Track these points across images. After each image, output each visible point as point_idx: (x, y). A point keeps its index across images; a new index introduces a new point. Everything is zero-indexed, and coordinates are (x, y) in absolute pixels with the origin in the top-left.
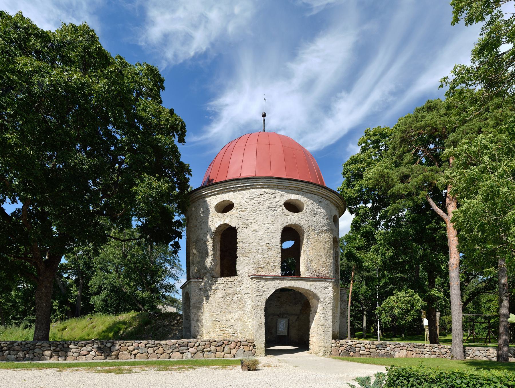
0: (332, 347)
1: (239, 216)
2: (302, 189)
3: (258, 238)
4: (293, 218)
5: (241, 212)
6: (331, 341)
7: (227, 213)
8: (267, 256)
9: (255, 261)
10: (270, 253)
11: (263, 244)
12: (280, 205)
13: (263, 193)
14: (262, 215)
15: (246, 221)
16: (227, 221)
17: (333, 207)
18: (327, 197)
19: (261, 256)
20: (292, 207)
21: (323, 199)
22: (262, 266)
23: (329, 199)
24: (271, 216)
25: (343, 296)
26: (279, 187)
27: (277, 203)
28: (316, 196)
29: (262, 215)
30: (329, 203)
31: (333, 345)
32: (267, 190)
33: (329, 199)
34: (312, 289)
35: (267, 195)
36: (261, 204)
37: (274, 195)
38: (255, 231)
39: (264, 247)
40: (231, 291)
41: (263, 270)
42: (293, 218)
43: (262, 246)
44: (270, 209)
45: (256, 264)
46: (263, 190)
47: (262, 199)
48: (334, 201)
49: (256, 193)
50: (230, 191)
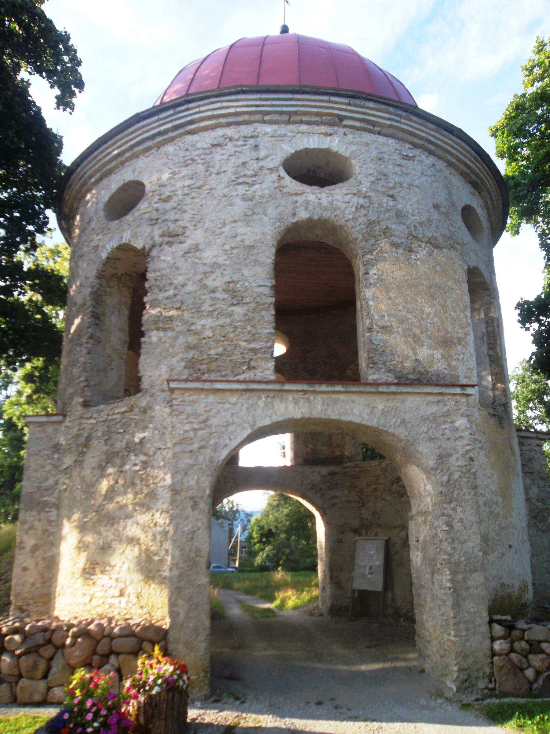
0: (493, 654)
1: (155, 215)
2: (341, 118)
3: (201, 269)
4: (313, 202)
5: (161, 205)
6: (485, 628)
7: (129, 217)
8: (228, 320)
9: (191, 339)
10: (239, 310)
11: (217, 283)
12: (271, 166)
13: (220, 140)
14: (215, 202)
15: (170, 224)
16: (126, 237)
17: (456, 181)
18: (431, 147)
19: (208, 322)
20: (316, 171)
21: (417, 152)
22: (212, 352)
23: (439, 152)
24: (243, 199)
25: (530, 460)
26: (267, 118)
27: (261, 163)
28: (391, 141)
29: (215, 202)
30: (441, 165)
31: (498, 646)
32: (230, 132)
33: (439, 152)
34: (392, 426)
35: (230, 146)
36: (214, 171)
37: (251, 141)
38: (196, 248)
39: (220, 295)
40: (120, 445)
41: (213, 366)
42: (313, 202)
43: (213, 291)
44: (241, 180)
45: (195, 347)
46: (220, 132)
47: (218, 156)
48: (459, 160)
49: (199, 145)
50: (136, 156)
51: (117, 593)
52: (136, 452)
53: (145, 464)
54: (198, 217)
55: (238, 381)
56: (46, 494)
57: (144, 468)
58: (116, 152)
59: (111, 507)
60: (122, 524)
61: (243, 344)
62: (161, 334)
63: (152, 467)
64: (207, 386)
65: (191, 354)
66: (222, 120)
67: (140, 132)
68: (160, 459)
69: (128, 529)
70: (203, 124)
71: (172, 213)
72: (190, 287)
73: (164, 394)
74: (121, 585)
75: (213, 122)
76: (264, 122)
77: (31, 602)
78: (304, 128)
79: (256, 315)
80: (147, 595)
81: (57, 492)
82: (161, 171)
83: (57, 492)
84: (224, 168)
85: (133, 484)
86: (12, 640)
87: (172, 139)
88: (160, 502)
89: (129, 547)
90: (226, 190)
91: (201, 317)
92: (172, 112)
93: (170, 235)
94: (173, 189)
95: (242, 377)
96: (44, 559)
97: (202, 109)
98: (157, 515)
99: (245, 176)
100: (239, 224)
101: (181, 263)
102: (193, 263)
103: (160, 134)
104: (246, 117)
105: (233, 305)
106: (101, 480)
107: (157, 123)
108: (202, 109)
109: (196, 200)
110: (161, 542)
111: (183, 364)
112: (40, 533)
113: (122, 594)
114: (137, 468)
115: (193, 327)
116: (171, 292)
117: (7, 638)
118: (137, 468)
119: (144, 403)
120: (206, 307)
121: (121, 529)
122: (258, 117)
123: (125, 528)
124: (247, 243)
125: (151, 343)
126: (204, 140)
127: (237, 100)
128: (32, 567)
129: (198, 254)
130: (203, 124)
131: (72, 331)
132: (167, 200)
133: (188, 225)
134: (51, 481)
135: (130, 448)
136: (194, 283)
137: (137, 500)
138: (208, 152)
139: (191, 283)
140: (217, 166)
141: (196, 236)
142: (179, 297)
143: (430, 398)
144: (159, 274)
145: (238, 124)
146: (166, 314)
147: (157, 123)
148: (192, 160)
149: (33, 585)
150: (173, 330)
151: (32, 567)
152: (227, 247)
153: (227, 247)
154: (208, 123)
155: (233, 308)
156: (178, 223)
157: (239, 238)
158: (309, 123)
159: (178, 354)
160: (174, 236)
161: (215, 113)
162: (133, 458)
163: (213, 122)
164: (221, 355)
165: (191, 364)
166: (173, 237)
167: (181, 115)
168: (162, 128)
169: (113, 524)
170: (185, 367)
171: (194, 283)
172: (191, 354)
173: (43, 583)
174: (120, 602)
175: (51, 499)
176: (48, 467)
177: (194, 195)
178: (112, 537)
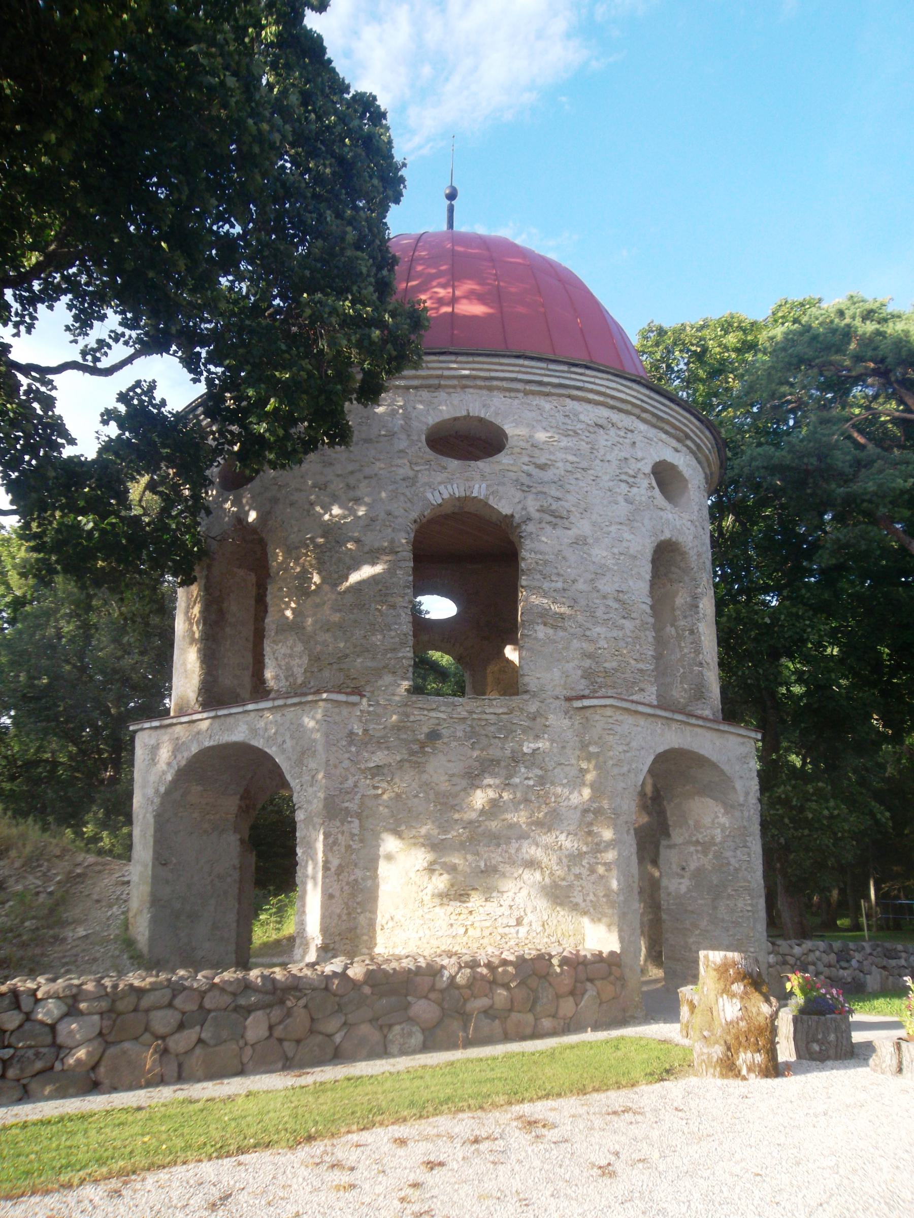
8: (621, 634)
9: (588, 647)
15: (550, 500)
26: (644, 415)
32: (615, 417)
35: (613, 432)
44: (623, 477)
47: (602, 440)
49: (582, 417)
51: (513, 922)
52: (527, 764)
53: (542, 781)
54: (583, 505)
55: (632, 702)
56: (347, 798)
57: (543, 784)
58: (467, 372)
59: (494, 825)
60: (514, 845)
61: (633, 662)
62: (550, 631)
63: (553, 783)
64: (633, 707)
65: (587, 663)
66: (611, 402)
67: (517, 369)
68: (562, 776)
69: (524, 851)
70: (591, 396)
71: (553, 486)
72: (581, 586)
73: (557, 702)
74: (516, 914)
75: (601, 399)
76: (638, 417)
77: (337, 939)
78: (664, 436)
79: (642, 635)
80: (555, 922)
81: (358, 796)
82: (533, 427)
83: (358, 796)
84: (608, 457)
85: (527, 801)
86: (505, 972)
87: (548, 394)
88: (566, 823)
89: (527, 871)
90: (611, 484)
91: (596, 623)
92: (565, 368)
93: (553, 513)
94: (552, 457)
95: (634, 698)
96: (348, 883)
97: (597, 381)
98: (562, 837)
99: (626, 473)
100: (624, 528)
101: (568, 553)
102: (582, 557)
103: (540, 383)
104: (629, 407)
105: (624, 618)
106: (471, 792)
107: (543, 372)
108: (597, 381)
109: (581, 484)
110: (569, 867)
111: (580, 672)
112: (343, 850)
113: (519, 922)
114: (531, 783)
115: (588, 633)
116: (560, 585)
117: (500, 970)
118: (531, 783)
119: (533, 708)
120: (599, 613)
121: (513, 851)
122: (637, 411)
123: (518, 850)
124: (632, 551)
125: (536, 639)
126: (590, 414)
127: (629, 388)
128: (337, 894)
129: (586, 548)
130: (591, 396)
131: (355, 578)
132: (542, 467)
133: (573, 509)
134: (350, 783)
135: (517, 759)
136: (585, 582)
137: (534, 819)
138: (591, 429)
139: (582, 580)
140: (602, 452)
141: (582, 527)
142: (569, 594)
143: (741, 740)
144: (541, 557)
145: (620, 410)
146: (555, 608)
147: (543, 372)
148: (575, 432)
149: (339, 916)
150: (566, 630)
151: (337, 894)
152: (616, 551)
153: (616, 551)
154: (596, 397)
155: (623, 621)
156: (560, 503)
157: (625, 544)
158: (666, 432)
159: (573, 659)
160: (556, 517)
161: (608, 391)
162: (523, 770)
163: (601, 399)
164: (616, 670)
165: (588, 675)
166: (557, 518)
167: (573, 376)
168: (546, 379)
169: (498, 845)
170: (582, 677)
171: (585, 582)
172: (587, 663)
173: (349, 914)
174: (517, 932)
175: (353, 806)
176: (347, 763)
177: (579, 475)
178: (500, 859)
